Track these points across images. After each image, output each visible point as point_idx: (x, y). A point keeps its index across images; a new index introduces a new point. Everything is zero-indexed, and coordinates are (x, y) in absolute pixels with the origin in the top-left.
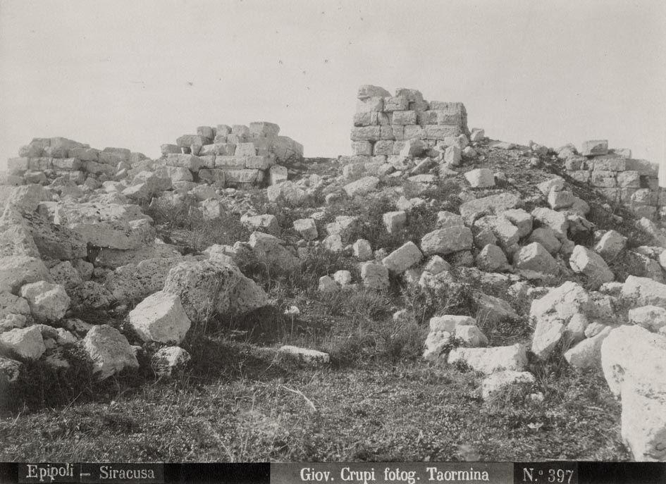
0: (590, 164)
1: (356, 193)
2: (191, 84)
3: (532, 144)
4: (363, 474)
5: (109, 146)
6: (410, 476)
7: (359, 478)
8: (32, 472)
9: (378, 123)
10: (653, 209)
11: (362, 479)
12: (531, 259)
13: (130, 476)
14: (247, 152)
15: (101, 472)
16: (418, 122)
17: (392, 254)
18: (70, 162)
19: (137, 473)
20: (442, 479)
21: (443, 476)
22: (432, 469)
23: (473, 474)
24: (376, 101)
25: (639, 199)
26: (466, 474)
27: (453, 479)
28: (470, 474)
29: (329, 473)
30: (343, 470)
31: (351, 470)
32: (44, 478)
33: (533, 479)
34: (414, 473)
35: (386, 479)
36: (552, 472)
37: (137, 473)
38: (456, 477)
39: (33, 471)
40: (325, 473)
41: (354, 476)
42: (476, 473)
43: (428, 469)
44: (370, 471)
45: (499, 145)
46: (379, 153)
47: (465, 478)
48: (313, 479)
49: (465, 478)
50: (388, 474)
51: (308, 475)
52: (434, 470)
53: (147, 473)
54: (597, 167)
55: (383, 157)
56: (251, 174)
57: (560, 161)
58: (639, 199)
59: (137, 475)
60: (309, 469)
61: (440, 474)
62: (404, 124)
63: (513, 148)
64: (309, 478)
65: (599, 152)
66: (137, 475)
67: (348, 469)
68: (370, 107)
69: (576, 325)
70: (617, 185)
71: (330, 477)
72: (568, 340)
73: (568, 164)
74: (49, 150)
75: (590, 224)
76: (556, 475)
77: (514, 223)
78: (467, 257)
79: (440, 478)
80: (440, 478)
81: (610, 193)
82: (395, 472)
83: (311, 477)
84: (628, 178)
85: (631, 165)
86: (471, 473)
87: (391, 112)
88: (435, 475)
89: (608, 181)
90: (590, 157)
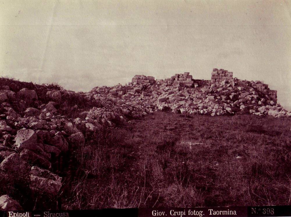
0: (257, 85)
1: (220, 91)
3: (246, 80)
4: (180, 213)
5: (149, 76)
6: (200, 213)
7: (231, 212)
11: (179, 214)
14: (189, 80)
16: (225, 76)
18: (148, 81)
20: (215, 214)
22: (211, 210)
23: (229, 212)
24: (217, 72)
25: (265, 91)
27: (220, 214)
28: (17, 214)
29: (164, 212)
30: (171, 211)
31: (175, 211)
34: (202, 212)
35: (189, 214)
36: (264, 209)
38: (222, 213)
39: (11, 214)
40: (163, 212)
41: (176, 214)
42: (230, 211)
43: (209, 210)
45: (240, 81)
46: (217, 82)
50: (190, 212)
51: (155, 214)
52: (212, 210)
53: (65, 214)
54: (258, 85)
55: (218, 82)
56: (191, 85)
57: (251, 84)
58: (265, 91)
61: (214, 212)
62: (222, 76)
63: (243, 81)
64: (155, 215)
65: (259, 83)
67: (173, 211)
68: (215, 73)
69: (265, 110)
70: (261, 89)
71: (165, 214)
72: (265, 112)
73: (253, 85)
74: (141, 78)
75: (260, 97)
76: (266, 211)
77: (250, 97)
78: (246, 103)
79: (214, 214)
80: (214, 214)
81: (260, 90)
82: (26, 214)
83: (157, 214)
84: (263, 87)
85: (264, 85)
86: (228, 211)
87: (220, 74)
88: (212, 212)
89: (260, 88)
90: (256, 84)
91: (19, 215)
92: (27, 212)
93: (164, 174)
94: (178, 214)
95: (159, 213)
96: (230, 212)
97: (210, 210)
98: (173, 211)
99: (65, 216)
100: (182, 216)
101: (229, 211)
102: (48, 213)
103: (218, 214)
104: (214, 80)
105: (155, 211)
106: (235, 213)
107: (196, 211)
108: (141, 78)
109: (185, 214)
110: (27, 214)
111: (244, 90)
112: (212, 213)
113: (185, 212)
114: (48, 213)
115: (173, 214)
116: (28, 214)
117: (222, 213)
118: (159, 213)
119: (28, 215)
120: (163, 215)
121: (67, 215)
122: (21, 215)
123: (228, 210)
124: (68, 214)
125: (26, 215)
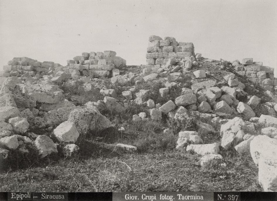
0: (245, 68)
1: (148, 80)
2: (79, 35)
3: (221, 60)
4: (151, 197)
5: (46, 61)
6: (171, 198)
7: (149, 198)
8: (13, 196)
10: (271, 87)
11: (150, 199)
12: (221, 108)
13: (54, 198)
14: (103, 63)
16: (174, 51)
17: (163, 105)
18: (29, 67)
19: (57, 196)
20: (184, 199)
21: (184, 198)
22: (179, 195)
23: (197, 197)
24: (156, 42)
25: (266, 83)
26: (194, 197)
27: (189, 199)
28: (195, 197)
29: (137, 196)
30: (143, 195)
31: (146, 195)
32: (18, 198)
33: (222, 199)
34: (172, 196)
35: (161, 199)
36: (230, 196)
37: (57, 196)
38: (190, 198)
39: (14, 196)
40: (135, 196)
41: (147, 198)
42: (198, 196)
43: (178, 195)
44: (154, 196)
45: (208, 60)
46: (158, 64)
47: (194, 198)
48: (130, 199)
49: (194, 198)
50: (161, 197)
51: (128, 197)
52: (180, 195)
53: (61, 196)
54: (248, 69)
55: (159, 65)
56: (104, 72)
57: (233, 67)
58: (266, 83)
59: (57, 197)
60: (128, 195)
61: (183, 197)
62: (168, 52)
63: (214, 61)
64: (128, 198)
65: (249, 63)
66: (57, 197)
67: (145, 195)
68: (154, 45)
70: (257, 77)
71: (137, 198)
73: (236, 68)
74: (20, 62)
77: (214, 93)
79: (183, 198)
80: (183, 198)
81: (254, 80)
82: (164, 196)
83: (129, 198)
84: (261, 74)
85: (262, 68)
86: (196, 196)
87: (163, 47)
88: (181, 197)
89: (253, 75)
90: (245, 65)
91: (166, 197)
103: (163, 198)
108: (20, 62)
113: (30, 195)
116: (60, 197)
123: (155, 195)
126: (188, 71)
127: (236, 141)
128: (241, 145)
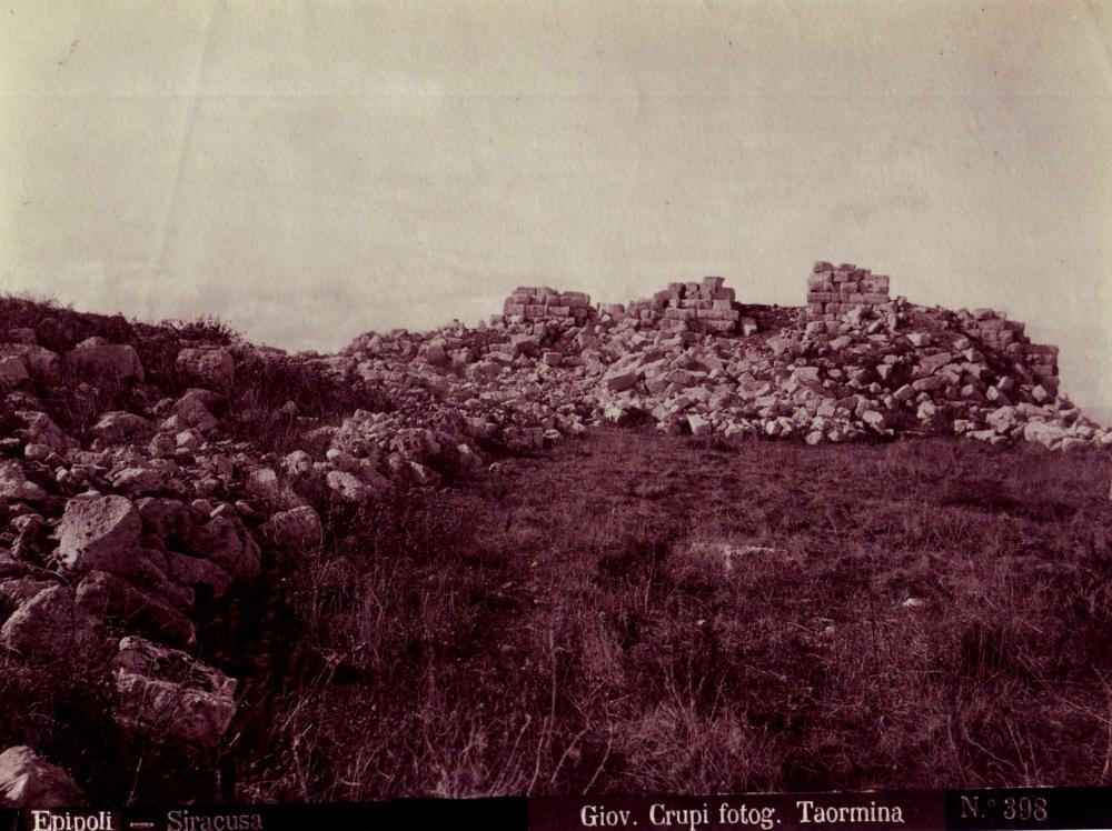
0: (980, 324)
1: (840, 348)
2: (60, 63)
3: (938, 307)
4: (689, 815)
5: (569, 290)
6: (765, 818)
7: (884, 811)
9: (829, 290)
10: (1021, 356)
11: (686, 821)
14: (724, 307)
15: (170, 822)
16: (859, 290)
18: (566, 310)
20: (823, 819)
22: (805, 804)
23: (877, 812)
24: (827, 274)
25: (1013, 350)
27: (842, 819)
29: (628, 812)
30: (653, 808)
31: (667, 808)
34: (771, 812)
35: (722, 821)
36: (1010, 802)
38: (847, 816)
39: (44, 820)
40: (621, 812)
41: (673, 819)
42: (880, 809)
43: (798, 803)
45: (919, 309)
46: (830, 312)
50: (726, 814)
51: (594, 818)
52: (809, 805)
53: (249, 820)
54: (985, 326)
55: (832, 315)
56: (729, 324)
57: (960, 321)
58: (1013, 350)
61: (820, 812)
62: (848, 291)
63: (929, 311)
64: (594, 822)
65: (989, 316)
67: (662, 807)
68: (823, 278)
70: (999, 340)
71: (630, 820)
73: (965, 324)
79: (819, 818)
80: (819, 818)
81: (994, 345)
82: (739, 809)
83: (598, 820)
84: (1006, 335)
85: (1008, 325)
86: (873, 809)
87: (839, 283)
88: (811, 813)
89: (992, 337)
90: (980, 320)
92: (102, 814)
93: (627, 665)
94: (682, 819)
95: (608, 817)
96: (880, 813)
97: (801, 806)
98: (662, 807)
99: (250, 828)
100: (696, 827)
101: (876, 807)
102: (183, 815)
104: (819, 307)
105: (594, 809)
106: (896, 817)
107: (748, 808)
109: (706, 821)
110: (102, 819)
111: (933, 343)
112: (811, 816)
113: (705, 811)
114: (183, 815)
115: (661, 820)
117: (847, 816)
118: (608, 817)
119: (109, 822)
120: (625, 822)
121: (256, 824)
122: (80, 823)
124: (259, 820)
125: (99, 822)
126: (896, 333)
127: (1012, 428)
128: (1016, 430)
